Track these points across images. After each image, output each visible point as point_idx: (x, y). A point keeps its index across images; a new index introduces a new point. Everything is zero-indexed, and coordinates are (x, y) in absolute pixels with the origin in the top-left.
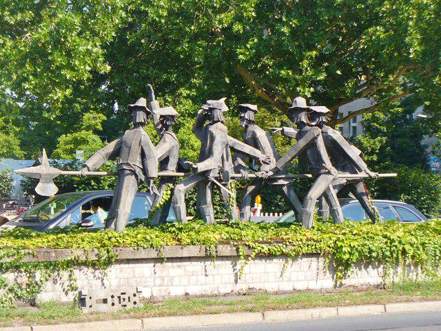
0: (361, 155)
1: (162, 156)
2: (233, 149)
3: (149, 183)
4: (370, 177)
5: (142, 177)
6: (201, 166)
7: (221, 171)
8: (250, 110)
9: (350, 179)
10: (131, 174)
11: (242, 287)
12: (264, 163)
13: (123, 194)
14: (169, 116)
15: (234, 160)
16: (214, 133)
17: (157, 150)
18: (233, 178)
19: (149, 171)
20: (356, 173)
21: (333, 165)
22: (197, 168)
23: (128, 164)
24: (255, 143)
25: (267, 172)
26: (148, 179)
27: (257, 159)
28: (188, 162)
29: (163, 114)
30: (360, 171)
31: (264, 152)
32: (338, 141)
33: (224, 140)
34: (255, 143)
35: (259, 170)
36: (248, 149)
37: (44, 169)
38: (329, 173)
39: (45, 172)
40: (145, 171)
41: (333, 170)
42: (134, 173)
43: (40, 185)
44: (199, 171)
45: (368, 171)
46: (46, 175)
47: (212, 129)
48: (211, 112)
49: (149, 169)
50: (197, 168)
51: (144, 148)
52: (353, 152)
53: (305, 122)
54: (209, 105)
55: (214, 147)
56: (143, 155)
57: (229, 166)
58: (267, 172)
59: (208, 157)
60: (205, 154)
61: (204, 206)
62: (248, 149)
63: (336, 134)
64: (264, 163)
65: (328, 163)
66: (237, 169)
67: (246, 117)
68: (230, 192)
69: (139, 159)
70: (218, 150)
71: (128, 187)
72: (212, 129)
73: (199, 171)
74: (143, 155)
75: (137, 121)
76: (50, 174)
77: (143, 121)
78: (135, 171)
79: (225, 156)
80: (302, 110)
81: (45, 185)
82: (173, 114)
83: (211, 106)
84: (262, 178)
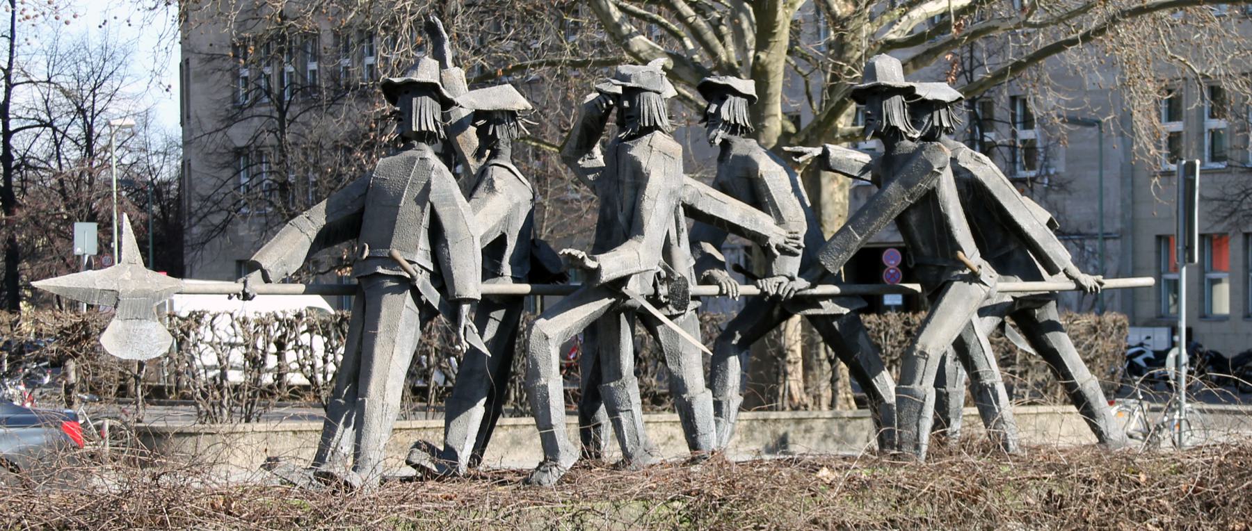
0: (1051, 224)
1: (490, 231)
2: (691, 211)
3: (455, 318)
4: (1080, 287)
5: (433, 296)
6: (610, 265)
7: (667, 276)
8: (736, 93)
9: (1018, 295)
10: (398, 290)
11: (242, 280)
12: (783, 251)
13: (378, 351)
14: (503, 112)
15: (694, 244)
16: (644, 164)
17: (475, 210)
18: (696, 298)
19: (457, 283)
20: (1039, 278)
21: (984, 256)
22: (598, 270)
23: (392, 262)
24: (756, 195)
25: (792, 279)
26: (452, 305)
27: (759, 239)
28: (574, 252)
29: (484, 107)
30: (1053, 270)
31: (780, 220)
32: (990, 185)
33: (674, 185)
34: (756, 195)
35: (768, 274)
36: (734, 210)
37: (127, 275)
38: (974, 278)
39: (132, 287)
40: (441, 277)
41: (987, 271)
42: (408, 284)
43: (115, 326)
44: (1048, 216)
45: (1075, 271)
46: (134, 295)
47: (638, 150)
48: (632, 102)
49: (455, 273)
50: (597, 271)
51: (440, 210)
52: (1031, 217)
53: (902, 128)
54: (626, 78)
55: (647, 205)
56: (436, 232)
57: (684, 263)
58: (792, 279)
59: (626, 237)
60: (619, 225)
61: (612, 385)
62: (734, 210)
63: (989, 172)
64: (783, 251)
65: (970, 253)
66: (704, 264)
67: (725, 115)
68: (687, 341)
69: (424, 244)
70: (658, 214)
71: (392, 329)
72: (638, 150)
73: (1048, 216)
74: (436, 232)
75: (415, 128)
76: (146, 294)
77: (432, 128)
78: (413, 279)
79: (673, 234)
80: (892, 91)
81: (133, 325)
82: (516, 107)
83: (632, 84)
84: (777, 296)
